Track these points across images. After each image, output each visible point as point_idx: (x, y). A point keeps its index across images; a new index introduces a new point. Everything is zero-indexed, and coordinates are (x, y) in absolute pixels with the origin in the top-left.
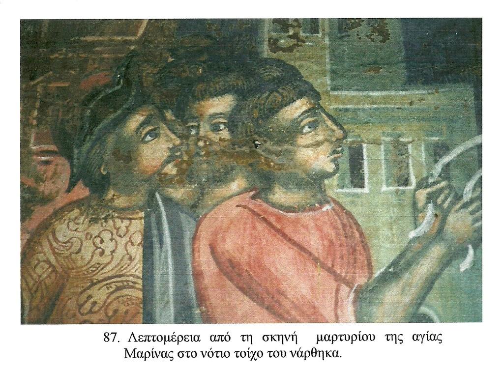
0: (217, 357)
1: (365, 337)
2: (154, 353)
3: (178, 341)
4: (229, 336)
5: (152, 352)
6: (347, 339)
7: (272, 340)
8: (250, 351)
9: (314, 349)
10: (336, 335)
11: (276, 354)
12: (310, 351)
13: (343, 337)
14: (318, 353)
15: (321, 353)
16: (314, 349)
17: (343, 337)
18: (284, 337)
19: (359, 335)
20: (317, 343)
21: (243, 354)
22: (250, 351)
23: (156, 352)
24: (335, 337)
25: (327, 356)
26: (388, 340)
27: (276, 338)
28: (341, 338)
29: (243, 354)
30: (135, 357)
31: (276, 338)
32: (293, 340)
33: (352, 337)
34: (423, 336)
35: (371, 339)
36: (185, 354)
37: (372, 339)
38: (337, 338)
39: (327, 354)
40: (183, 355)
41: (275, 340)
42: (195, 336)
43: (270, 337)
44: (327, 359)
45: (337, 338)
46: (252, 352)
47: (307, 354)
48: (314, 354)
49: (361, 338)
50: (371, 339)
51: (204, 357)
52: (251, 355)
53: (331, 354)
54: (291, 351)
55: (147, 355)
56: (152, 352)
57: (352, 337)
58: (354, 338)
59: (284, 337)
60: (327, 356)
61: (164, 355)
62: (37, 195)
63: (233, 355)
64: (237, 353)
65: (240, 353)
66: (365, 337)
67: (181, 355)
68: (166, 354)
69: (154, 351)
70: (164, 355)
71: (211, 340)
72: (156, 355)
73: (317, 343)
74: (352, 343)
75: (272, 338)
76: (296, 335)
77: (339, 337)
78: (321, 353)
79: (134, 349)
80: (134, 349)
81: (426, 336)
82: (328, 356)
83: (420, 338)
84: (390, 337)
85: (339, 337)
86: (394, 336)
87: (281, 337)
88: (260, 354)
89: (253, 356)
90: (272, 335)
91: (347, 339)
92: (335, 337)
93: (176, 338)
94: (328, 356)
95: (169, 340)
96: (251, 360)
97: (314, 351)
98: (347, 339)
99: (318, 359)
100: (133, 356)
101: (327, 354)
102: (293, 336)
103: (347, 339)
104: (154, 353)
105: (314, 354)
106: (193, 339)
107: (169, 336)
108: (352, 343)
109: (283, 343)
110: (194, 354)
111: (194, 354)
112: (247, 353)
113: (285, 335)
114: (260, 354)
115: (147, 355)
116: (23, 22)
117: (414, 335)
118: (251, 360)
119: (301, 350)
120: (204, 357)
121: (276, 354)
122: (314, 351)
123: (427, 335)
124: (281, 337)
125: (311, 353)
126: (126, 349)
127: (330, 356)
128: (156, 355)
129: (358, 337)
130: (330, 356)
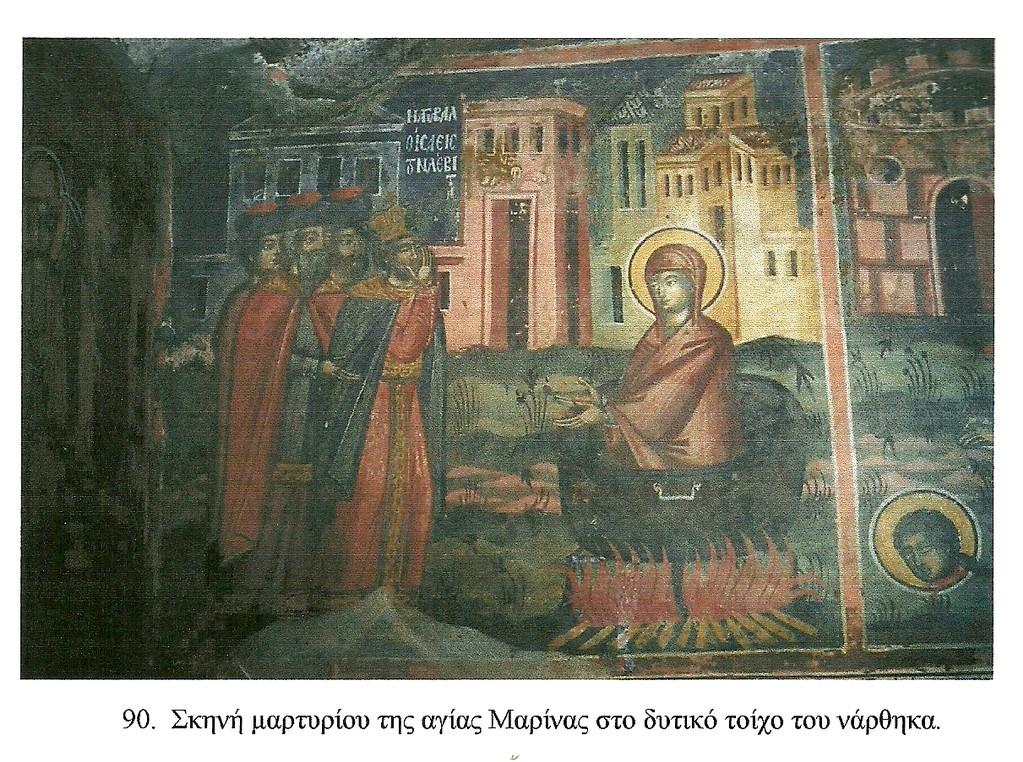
0: (677, 727)
1: (349, 722)
2: (550, 720)
3: (284, 727)
4: (714, 718)
5: (547, 717)
6: (314, 724)
7: (191, 727)
8: (757, 715)
9: (885, 713)
10: (291, 717)
11: (809, 722)
12: (878, 717)
13: (305, 721)
14: (893, 721)
15: (900, 721)
16: (885, 713)
17: (305, 721)
18: (217, 720)
19: (338, 717)
20: (254, 732)
21: (743, 722)
22: (757, 715)
23: (553, 717)
24: (288, 720)
25: (910, 727)
26: (731, 727)
27: (201, 722)
28: (300, 723)
29: (743, 722)
30: (510, 727)
31: (201, 722)
32: (233, 727)
33: (323, 721)
34: (442, 719)
35: (360, 725)
36: (612, 722)
37: (364, 725)
38: (293, 723)
39: (912, 722)
40: (607, 723)
41: (198, 727)
42: (517, 718)
43: (690, 721)
44: (911, 732)
45: (293, 723)
46: (761, 717)
47: (872, 722)
48: (885, 723)
49: (341, 724)
50: (360, 725)
51: (843, 727)
52: (759, 723)
53: (919, 722)
54: (840, 717)
55: (536, 722)
56: (547, 717)
57: (323, 721)
58: (328, 722)
59: (217, 720)
60: (910, 727)
61: (569, 724)
62: (773, 547)
63: (789, 723)
64: (616, 720)
65: (736, 719)
66: (349, 722)
67: (603, 722)
68: (861, 721)
69: (549, 714)
70: (569, 724)
71: (646, 726)
72: (555, 723)
73: (254, 732)
74: (323, 733)
75: (694, 722)
76: (240, 717)
77: (297, 721)
78: (900, 721)
79: (509, 712)
80: (509, 712)
81: (449, 720)
82: (696, 726)
83: (437, 723)
84: (388, 721)
85: (297, 721)
86: (396, 720)
87: (210, 720)
88: (777, 722)
89: (763, 727)
90: (910, 717)
91: (314, 724)
92: (288, 720)
93: (864, 723)
94: (696, 726)
95: (234, 718)
96: (760, 733)
97: (885, 716)
98: (314, 725)
99: (893, 732)
100: (506, 724)
101: (912, 722)
102: (234, 718)
103: (314, 725)
104: (550, 720)
105: (885, 723)
106: (455, 724)
107: (262, 717)
108: (323, 733)
109: (213, 732)
110: (629, 722)
111: (629, 722)
112: (751, 720)
113: (219, 717)
114: (777, 722)
115: (536, 722)
116: (34, 50)
117: (424, 718)
118: (760, 733)
119: (859, 714)
120: (843, 727)
121: (809, 722)
122: (885, 716)
123: (452, 717)
124: (210, 720)
125: (879, 720)
126: (493, 712)
127: (699, 727)
128: (555, 723)
129: (335, 720)
130: (699, 727)
